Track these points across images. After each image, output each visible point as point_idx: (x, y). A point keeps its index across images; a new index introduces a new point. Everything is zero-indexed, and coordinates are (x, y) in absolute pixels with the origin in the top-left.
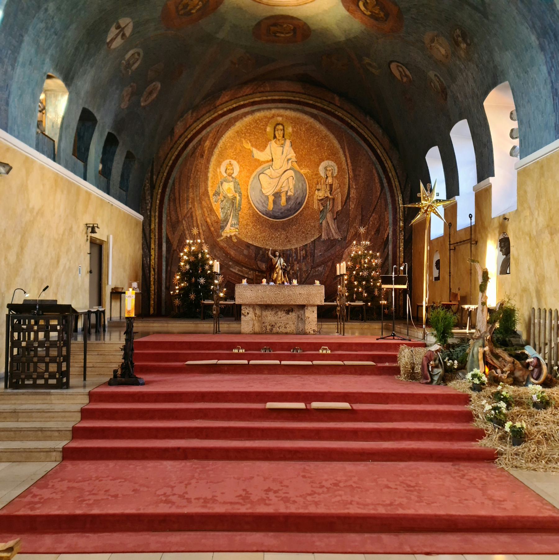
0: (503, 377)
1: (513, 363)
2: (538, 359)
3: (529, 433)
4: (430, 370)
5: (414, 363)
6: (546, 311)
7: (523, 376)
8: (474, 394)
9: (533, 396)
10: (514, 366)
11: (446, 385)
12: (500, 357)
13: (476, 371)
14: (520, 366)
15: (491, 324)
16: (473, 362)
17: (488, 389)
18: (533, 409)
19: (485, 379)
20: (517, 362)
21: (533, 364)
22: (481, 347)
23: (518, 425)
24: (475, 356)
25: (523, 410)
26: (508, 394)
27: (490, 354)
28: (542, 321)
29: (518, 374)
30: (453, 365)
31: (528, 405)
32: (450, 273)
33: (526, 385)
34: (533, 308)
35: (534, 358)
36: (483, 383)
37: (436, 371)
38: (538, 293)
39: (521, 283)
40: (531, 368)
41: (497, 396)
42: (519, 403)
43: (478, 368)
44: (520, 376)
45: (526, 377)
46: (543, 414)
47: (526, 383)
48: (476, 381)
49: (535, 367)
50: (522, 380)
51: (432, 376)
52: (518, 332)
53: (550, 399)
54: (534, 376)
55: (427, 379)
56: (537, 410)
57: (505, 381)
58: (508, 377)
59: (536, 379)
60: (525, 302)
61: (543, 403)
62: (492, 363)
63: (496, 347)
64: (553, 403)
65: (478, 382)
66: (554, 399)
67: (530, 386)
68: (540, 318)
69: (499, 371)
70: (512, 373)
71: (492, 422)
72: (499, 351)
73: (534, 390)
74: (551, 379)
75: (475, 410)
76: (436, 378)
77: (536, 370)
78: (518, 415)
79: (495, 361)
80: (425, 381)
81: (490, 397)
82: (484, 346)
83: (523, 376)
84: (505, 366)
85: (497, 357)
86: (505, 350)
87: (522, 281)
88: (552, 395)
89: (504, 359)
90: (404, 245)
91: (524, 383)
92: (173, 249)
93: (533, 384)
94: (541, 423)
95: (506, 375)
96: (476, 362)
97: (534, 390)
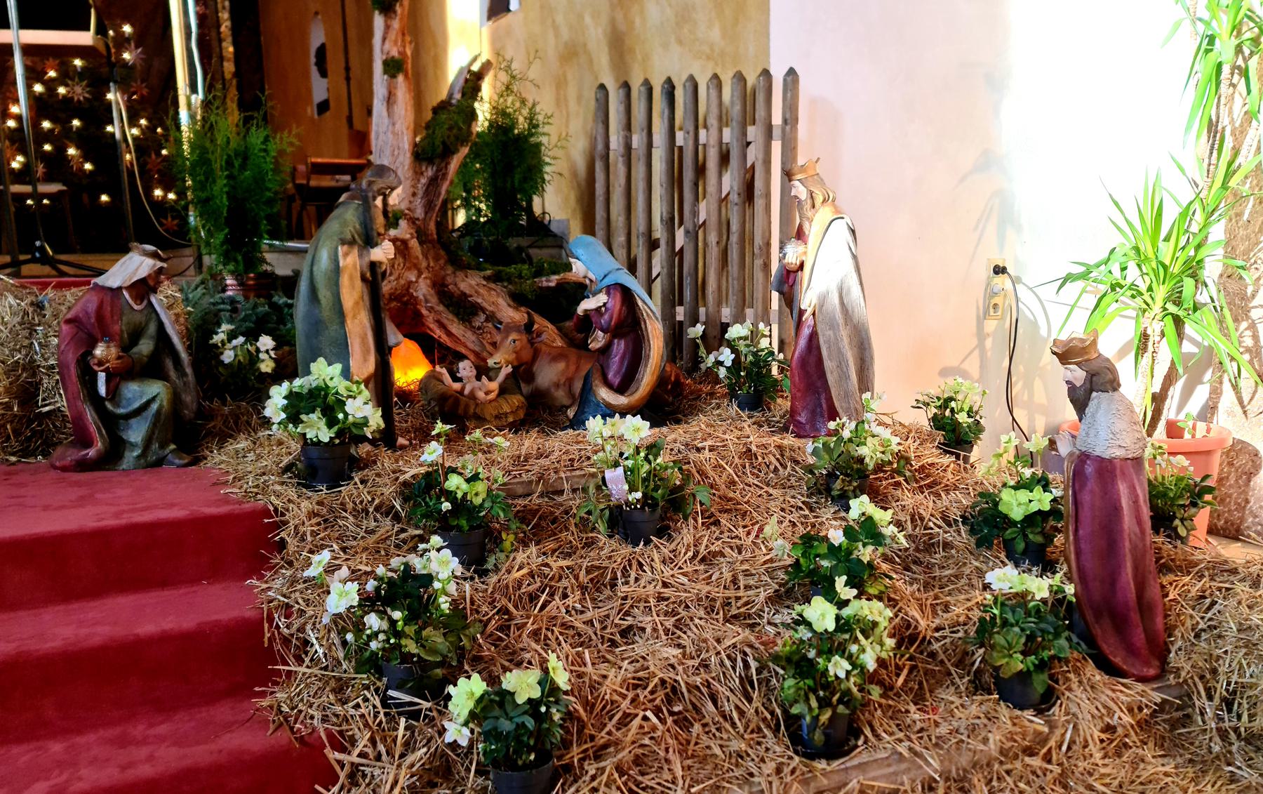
0: (481, 395)
1: (528, 327)
2: (627, 294)
3: (589, 706)
4: (102, 390)
5: (32, 367)
6: (650, 91)
7: (570, 381)
8: (299, 507)
9: (609, 474)
10: (531, 342)
11: (196, 461)
12: (476, 309)
13: (324, 372)
14: (559, 343)
15: (430, 161)
16: (316, 326)
17: (386, 460)
18: (613, 550)
19: (362, 409)
20: (540, 322)
21: (604, 321)
22: (352, 243)
23: (522, 684)
24: (324, 294)
25: (557, 563)
26: (481, 487)
27: (434, 301)
28: (637, 140)
29: (548, 374)
30: (254, 359)
31: (584, 525)
32: (347, 69)
33: (578, 423)
34: (602, 87)
35: (608, 290)
36: (350, 434)
37: (138, 392)
38: (619, 45)
39: (556, 29)
40: (598, 340)
41: (424, 502)
42: (540, 524)
43: (340, 353)
44: (557, 385)
45: (578, 386)
46: (662, 567)
47: (585, 405)
48: (318, 429)
49: (616, 331)
50: (566, 402)
51: (113, 424)
52: (553, 228)
53: (687, 477)
54: (610, 376)
55: (88, 444)
56: (626, 550)
57: (489, 412)
58: (503, 391)
59: (621, 389)
60: (572, 105)
61: (654, 506)
62: (445, 339)
63: (459, 265)
64: (703, 495)
65: (325, 435)
66: (702, 473)
67: (595, 424)
68: (628, 127)
69: (466, 368)
70: (522, 373)
71: (380, 673)
72: (470, 283)
73: (617, 436)
74: (678, 384)
75: (287, 610)
76: (136, 433)
77: (619, 347)
78: (533, 598)
79: (457, 328)
80: (72, 455)
81: (388, 511)
82: (368, 240)
83: (570, 381)
84: (494, 344)
85: (464, 308)
86: (496, 278)
87: (560, 19)
88: (693, 456)
89: (491, 318)
90: (233, 18)
91: (571, 413)
92: (93, 260)
93: (609, 412)
94: (647, 621)
95: (494, 385)
96: (333, 328)
97: (617, 436)
